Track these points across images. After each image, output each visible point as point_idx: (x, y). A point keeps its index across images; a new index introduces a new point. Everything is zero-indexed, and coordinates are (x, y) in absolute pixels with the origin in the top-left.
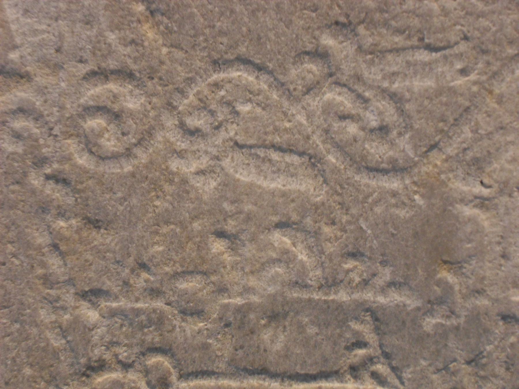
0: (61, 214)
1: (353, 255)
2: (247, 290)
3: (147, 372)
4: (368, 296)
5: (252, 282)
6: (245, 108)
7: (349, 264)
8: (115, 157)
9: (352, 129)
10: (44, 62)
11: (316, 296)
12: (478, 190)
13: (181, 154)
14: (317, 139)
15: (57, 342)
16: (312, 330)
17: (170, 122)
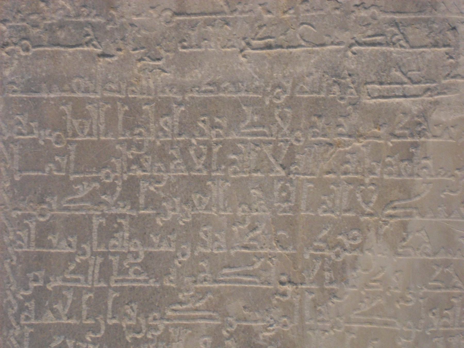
1: (84, 6)
2: (52, 18)
3: (22, 46)
5: (53, 16)
7: (83, 9)
11: (74, 20)
16: (73, 31)
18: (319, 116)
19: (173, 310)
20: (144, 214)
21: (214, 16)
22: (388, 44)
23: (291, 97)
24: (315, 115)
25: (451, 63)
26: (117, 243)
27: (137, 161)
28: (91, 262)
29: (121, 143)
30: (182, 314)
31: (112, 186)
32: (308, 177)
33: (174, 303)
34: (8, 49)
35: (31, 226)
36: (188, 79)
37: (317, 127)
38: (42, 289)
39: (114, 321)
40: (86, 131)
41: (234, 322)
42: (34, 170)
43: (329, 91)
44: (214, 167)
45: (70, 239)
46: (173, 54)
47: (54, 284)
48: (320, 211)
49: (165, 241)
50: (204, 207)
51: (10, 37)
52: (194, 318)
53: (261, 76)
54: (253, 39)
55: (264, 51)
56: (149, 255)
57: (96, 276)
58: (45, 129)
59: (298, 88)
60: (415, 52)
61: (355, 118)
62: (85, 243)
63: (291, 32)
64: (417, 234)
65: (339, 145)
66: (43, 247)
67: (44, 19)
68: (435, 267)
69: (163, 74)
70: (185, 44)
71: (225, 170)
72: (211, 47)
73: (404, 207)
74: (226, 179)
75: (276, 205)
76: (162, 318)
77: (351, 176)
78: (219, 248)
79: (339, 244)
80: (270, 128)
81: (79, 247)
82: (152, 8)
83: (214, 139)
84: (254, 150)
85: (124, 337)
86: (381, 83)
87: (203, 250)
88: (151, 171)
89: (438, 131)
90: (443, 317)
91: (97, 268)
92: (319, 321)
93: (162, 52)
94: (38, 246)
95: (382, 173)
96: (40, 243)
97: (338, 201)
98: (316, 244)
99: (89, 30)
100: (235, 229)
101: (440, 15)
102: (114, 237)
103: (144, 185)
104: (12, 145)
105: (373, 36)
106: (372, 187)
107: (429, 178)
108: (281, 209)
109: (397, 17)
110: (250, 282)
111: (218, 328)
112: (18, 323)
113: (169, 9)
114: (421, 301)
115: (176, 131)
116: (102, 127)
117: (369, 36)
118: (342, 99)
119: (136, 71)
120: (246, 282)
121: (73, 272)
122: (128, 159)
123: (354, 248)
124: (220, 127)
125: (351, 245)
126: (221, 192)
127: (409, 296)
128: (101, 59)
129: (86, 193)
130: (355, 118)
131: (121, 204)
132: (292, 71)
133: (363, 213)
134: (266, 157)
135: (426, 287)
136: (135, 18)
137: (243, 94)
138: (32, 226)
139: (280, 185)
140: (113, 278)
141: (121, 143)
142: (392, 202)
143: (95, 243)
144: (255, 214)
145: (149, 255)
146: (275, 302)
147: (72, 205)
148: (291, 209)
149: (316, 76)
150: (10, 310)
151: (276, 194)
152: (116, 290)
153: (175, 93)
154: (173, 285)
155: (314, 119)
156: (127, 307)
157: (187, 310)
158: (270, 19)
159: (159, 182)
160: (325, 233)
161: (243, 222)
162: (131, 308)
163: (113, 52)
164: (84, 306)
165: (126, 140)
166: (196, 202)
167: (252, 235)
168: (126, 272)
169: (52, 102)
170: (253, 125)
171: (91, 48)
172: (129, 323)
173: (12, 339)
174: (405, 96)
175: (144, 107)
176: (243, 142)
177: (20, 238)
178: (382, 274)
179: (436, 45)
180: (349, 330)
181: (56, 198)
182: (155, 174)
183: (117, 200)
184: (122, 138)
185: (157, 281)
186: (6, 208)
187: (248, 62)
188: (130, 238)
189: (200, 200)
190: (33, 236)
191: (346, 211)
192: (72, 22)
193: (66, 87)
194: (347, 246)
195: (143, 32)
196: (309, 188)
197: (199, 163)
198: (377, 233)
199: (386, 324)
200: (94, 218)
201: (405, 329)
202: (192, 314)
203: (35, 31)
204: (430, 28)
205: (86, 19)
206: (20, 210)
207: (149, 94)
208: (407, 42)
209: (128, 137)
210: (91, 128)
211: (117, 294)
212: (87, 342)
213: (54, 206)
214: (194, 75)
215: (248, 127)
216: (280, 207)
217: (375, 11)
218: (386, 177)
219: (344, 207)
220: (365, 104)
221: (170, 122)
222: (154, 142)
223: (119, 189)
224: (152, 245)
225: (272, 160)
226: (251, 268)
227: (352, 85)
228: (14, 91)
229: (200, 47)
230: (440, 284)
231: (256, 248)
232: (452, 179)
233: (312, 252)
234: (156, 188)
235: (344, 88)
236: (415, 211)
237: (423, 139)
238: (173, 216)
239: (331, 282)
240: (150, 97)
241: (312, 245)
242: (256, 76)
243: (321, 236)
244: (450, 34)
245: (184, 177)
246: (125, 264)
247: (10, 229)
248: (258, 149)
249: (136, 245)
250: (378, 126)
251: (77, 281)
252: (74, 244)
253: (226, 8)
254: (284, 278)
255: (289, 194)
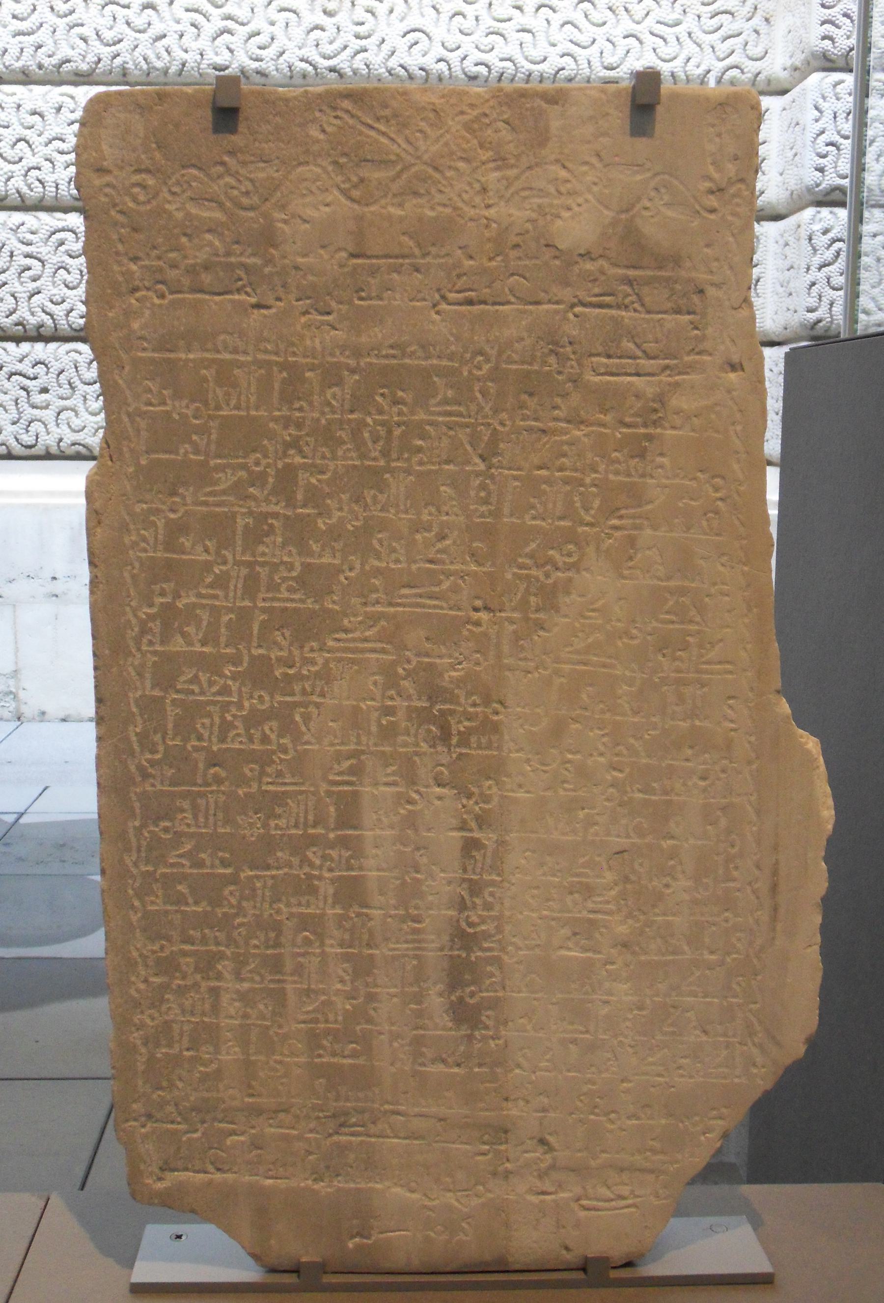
0: (123, 226)
1: (237, 243)
2: (196, 257)
3: (156, 291)
4: (243, 259)
5: (197, 254)
6: (194, 184)
7: (235, 246)
8: (144, 203)
9: (235, 192)
10: (117, 165)
11: (222, 259)
12: (284, 216)
13: (169, 202)
14: (222, 197)
15: (121, 279)
16: (221, 274)
17: (165, 189)
18: (531, 395)
19: (339, 640)
20: (302, 513)
21: (401, 261)
22: (618, 307)
23: (496, 368)
24: (526, 392)
25: (696, 335)
26: (267, 551)
27: (295, 444)
28: (234, 574)
29: (276, 420)
30: (347, 645)
31: (263, 475)
32: (515, 473)
33: (336, 631)
34: (138, 295)
35: (158, 523)
36: (364, 339)
37: (527, 408)
38: (166, 607)
39: (261, 651)
40: (233, 402)
41: (412, 657)
42: (166, 452)
43: (545, 363)
44: (394, 456)
45: (208, 543)
46: (347, 307)
47: (185, 601)
48: (527, 517)
49: (328, 550)
50: (379, 507)
51: (142, 280)
52: (363, 651)
53: (458, 338)
54: (450, 291)
55: (463, 308)
56: (307, 567)
57: (239, 593)
58: (181, 398)
59: (504, 357)
60: (652, 319)
61: (575, 399)
62: (226, 549)
63: (497, 285)
64: (647, 552)
65: (555, 432)
66: (174, 552)
67: (185, 257)
68: (667, 595)
69: (333, 333)
70: (363, 294)
71: (408, 460)
72: (395, 300)
73: (633, 517)
74: (408, 472)
75: (472, 507)
76: (321, 649)
77: (567, 473)
78: (397, 561)
79: (550, 561)
80: (467, 406)
81: (218, 553)
82: (323, 247)
83: (396, 419)
84: (445, 434)
85: (272, 672)
86: (609, 357)
87: (376, 563)
88: (313, 457)
89: (678, 421)
90: (675, 659)
91: (241, 581)
92: (520, 659)
93: (333, 304)
94: (167, 550)
95: (606, 472)
96: (170, 546)
97: (550, 506)
98: (520, 560)
99: (241, 273)
100: (418, 537)
101: (683, 273)
102: (263, 543)
103: (302, 475)
104: (138, 419)
105: (601, 295)
106: (594, 489)
107: (664, 481)
108: (478, 514)
109: (631, 273)
110: (435, 607)
111: (394, 664)
112: (139, 649)
113: (345, 249)
114: (649, 638)
115: (347, 406)
116: (253, 399)
117: (596, 295)
118: (559, 373)
119: (299, 327)
120: (430, 607)
121: (211, 586)
122: (284, 441)
123: (569, 567)
124: (404, 403)
125: (565, 563)
126: (402, 489)
127: (634, 631)
128: (255, 311)
129: (229, 483)
130: (575, 399)
131: (274, 500)
132: (497, 334)
133: (583, 523)
134: (462, 444)
135: (657, 620)
136: (300, 260)
137: (435, 362)
138: (161, 524)
139: (478, 482)
140: (261, 595)
141: (276, 420)
142: (618, 509)
143: (239, 549)
144: (445, 518)
145: (307, 567)
146: (465, 633)
147: (211, 499)
148: (490, 513)
149: (528, 342)
150: (129, 632)
151: (472, 493)
152: (264, 610)
153: (348, 357)
154: (337, 607)
155: (524, 397)
156: (277, 633)
157: (354, 640)
158: (472, 266)
159: (323, 473)
160: (533, 546)
161: (428, 529)
162: (283, 634)
163: (271, 302)
164: (223, 630)
165: (282, 417)
166: (368, 500)
167: (439, 546)
168: (275, 588)
169: (191, 365)
170: (446, 402)
171: (243, 297)
172: (279, 654)
173: (131, 669)
174: (638, 374)
175: (308, 374)
176: (431, 423)
177: (144, 539)
178: (600, 603)
179: (678, 311)
180: (557, 673)
181: (191, 489)
182: (319, 462)
183: (269, 494)
184: (277, 413)
185: (316, 601)
186: (129, 499)
187: (443, 320)
188: (284, 545)
189: (375, 497)
190: (160, 537)
191: (561, 518)
192: (220, 263)
193: (209, 346)
194: (560, 564)
195: (310, 278)
196: (515, 487)
197: (375, 450)
198: (598, 549)
199: (604, 666)
200: (239, 516)
201: (627, 673)
202: (360, 645)
203: (172, 274)
204: (672, 289)
205: (239, 259)
206: (146, 503)
207: (314, 358)
208: (643, 305)
209: (285, 412)
210: (239, 399)
211: (264, 617)
212: (226, 677)
213: (189, 500)
214: (372, 334)
215: (439, 404)
216: (476, 510)
217: (604, 263)
218: (611, 477)
219: (558, 514)
220: (588, 381)
221: (339, 393)
222: (318, 420)
223: (271, 480)
224: (311, 554)
225: (469, 448)
226: (437, 589)
227: (572, 356)
228: (144, 349)
229: (381, 299)
230: (674, 618)
231: (443, 562)
232: (694, 484)
233: (516, 570)
234: (319, 481)
235: (562, 359)
236: (645, 523)
237: (659, 430)
238: (339, 517)
239: (537, 610)
240: (316, 362)
241: (516, 560)
242: (452, 339)
243: (528, 550)
244: (696, 299)
245: (355, 466)
246: (276, 578)
247: (132, 527)
248: (452, 433)
249: (290, 554)
250: (605, 412)
251: (215, 597)
252: (212, 549)
253: (417, 251)
254: (478, 603)
255: (489, 494)
